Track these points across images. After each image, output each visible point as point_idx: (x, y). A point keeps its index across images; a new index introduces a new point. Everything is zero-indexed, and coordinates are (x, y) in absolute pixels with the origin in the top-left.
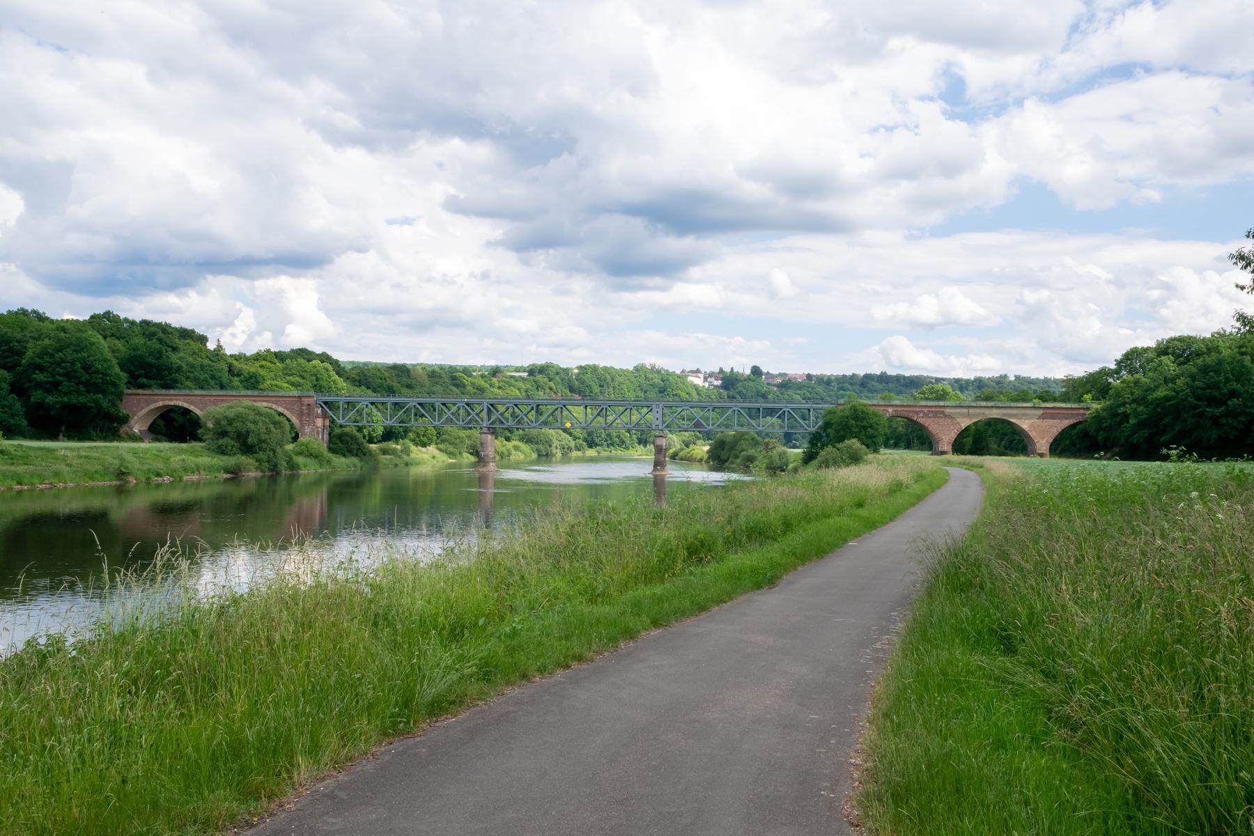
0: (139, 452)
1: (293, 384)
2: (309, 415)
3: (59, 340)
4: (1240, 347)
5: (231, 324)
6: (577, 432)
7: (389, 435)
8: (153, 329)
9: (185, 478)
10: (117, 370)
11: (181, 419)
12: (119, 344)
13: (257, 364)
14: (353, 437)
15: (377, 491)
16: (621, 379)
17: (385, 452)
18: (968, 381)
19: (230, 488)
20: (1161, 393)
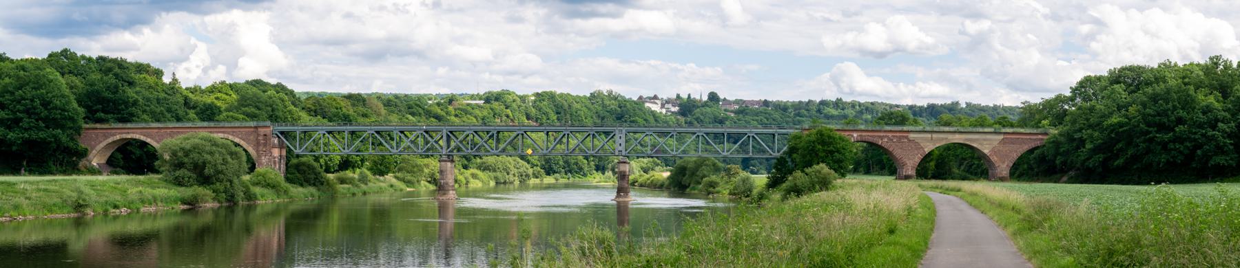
0: (97, 185)
1: (248, 115)
2: (265, 145)
3: (18, 78)
4: (1184, 78)
5: (186, 59)
6: (534, 160)
7: (346, 164)
8: (109, 65)
9: (142, 210)
10: (75, 105)
11: (138, 152)
12: (76, 81)
13: (213, 96)
14: (310, 167)
15: (335, 218)
16: (578, 106)
17: (342, 181)
18: (921, 108)
19: (187, 219)
20: (1115, 119)
